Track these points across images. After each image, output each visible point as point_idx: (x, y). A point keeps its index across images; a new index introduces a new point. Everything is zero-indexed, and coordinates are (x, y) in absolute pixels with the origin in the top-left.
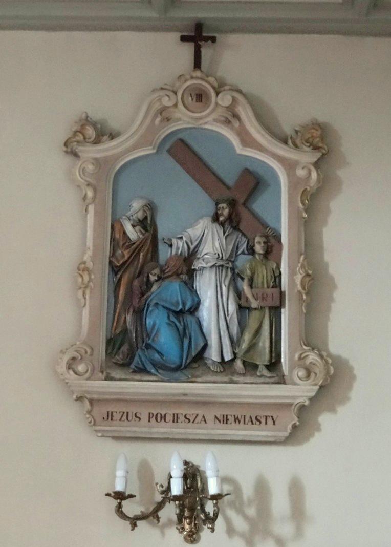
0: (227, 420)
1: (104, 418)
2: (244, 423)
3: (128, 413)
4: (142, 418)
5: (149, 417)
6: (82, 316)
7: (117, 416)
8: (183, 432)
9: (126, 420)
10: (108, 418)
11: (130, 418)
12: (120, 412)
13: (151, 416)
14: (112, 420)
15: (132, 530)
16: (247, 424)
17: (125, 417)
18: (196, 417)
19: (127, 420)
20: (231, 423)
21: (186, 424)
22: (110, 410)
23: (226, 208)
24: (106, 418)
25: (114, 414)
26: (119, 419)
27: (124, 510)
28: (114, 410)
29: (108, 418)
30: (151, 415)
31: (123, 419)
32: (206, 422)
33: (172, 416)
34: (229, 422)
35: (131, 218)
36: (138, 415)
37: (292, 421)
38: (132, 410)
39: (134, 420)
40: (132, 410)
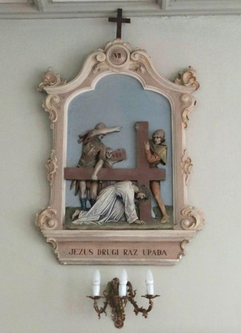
0: (75, 252)
1: (70, 253)
2: (108, 254)
3: (108, 250)
4: (93, 252)
5: (148, 252)
6: (50, 191)
7: (78, 252)
8: (90, 260)
9: (84, 254)
10: (72, 253)
11: (86, 253)
12: (80, 249)
13: (150, 252)
14: (74, 254)
15: (99, 319)
16: (128, 255)
17: (83, 252)
18: (136, 252)
19: (108, 254)
20: (82, 254)
21: (90, 255)
22: (74, 248)
23: (53, 122)
24: (71, 253)
25: (76, 250)
26: (79, 253)
27: (148, 305)
28: (75, 248)
29: (72, 253)
30: (99, 251)
31: (81, 253)
32: (166, 255)
33: (117, 251)
34: (76, 253)
35: (102, 136)
36: (91, 251)
37: (60, 254)
38: (87, 248)
39: (89, 254)
40: (87, 248)
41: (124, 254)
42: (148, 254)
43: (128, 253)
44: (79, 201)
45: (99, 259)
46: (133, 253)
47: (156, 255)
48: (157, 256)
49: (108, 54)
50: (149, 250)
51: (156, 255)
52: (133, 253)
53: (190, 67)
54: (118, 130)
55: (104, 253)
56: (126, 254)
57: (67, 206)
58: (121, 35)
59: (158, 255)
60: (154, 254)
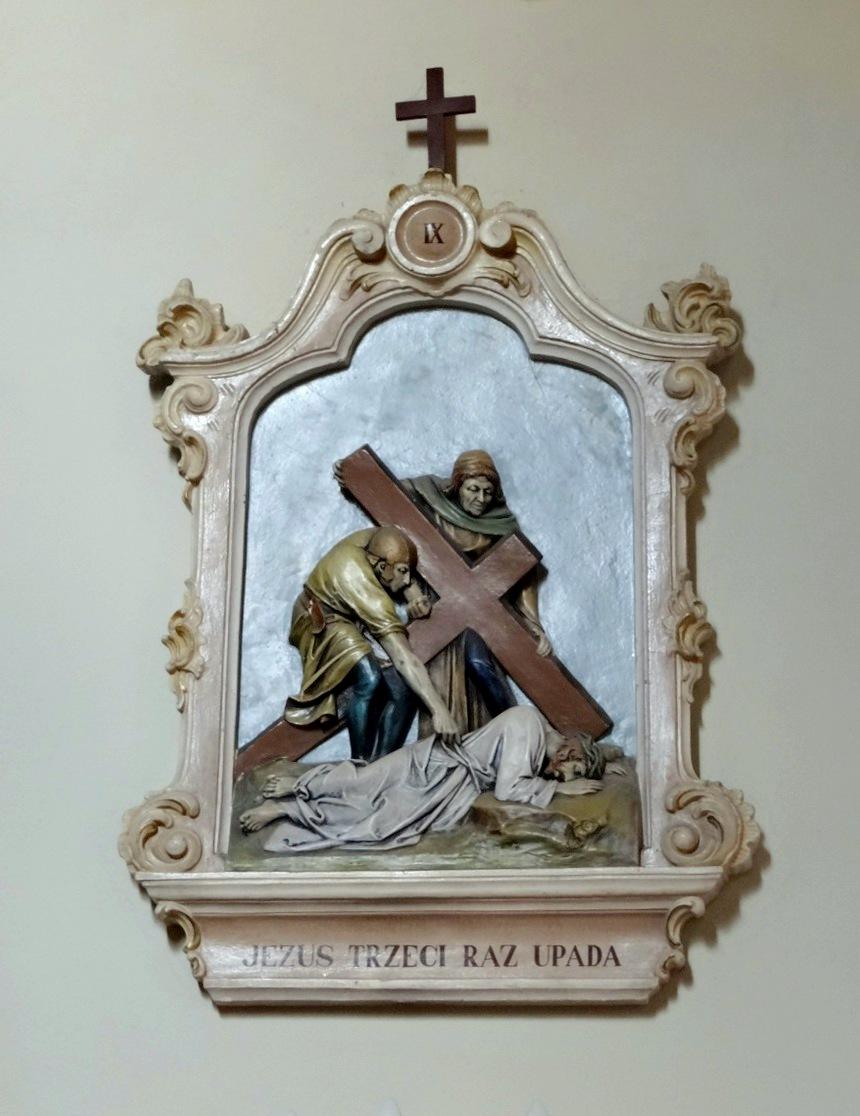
30: (595, 953)
41: (466, 965)
42: (555, 964)
43: (478, 959)
44: (271, 723)
45: (610, 981)
46: (501, 960)
47: (581, 964)
48: (587, 970)
49: (470, 239)
50: (555, 948)
51: (581, 964)
52: (501, 960)
53: (702, 266)
54: (609, 555)
55: (471, 958)
56: (474, 964)
57: (477, 805)
58: (428, 86)
59: (590, 964)
60: (575, 962)
